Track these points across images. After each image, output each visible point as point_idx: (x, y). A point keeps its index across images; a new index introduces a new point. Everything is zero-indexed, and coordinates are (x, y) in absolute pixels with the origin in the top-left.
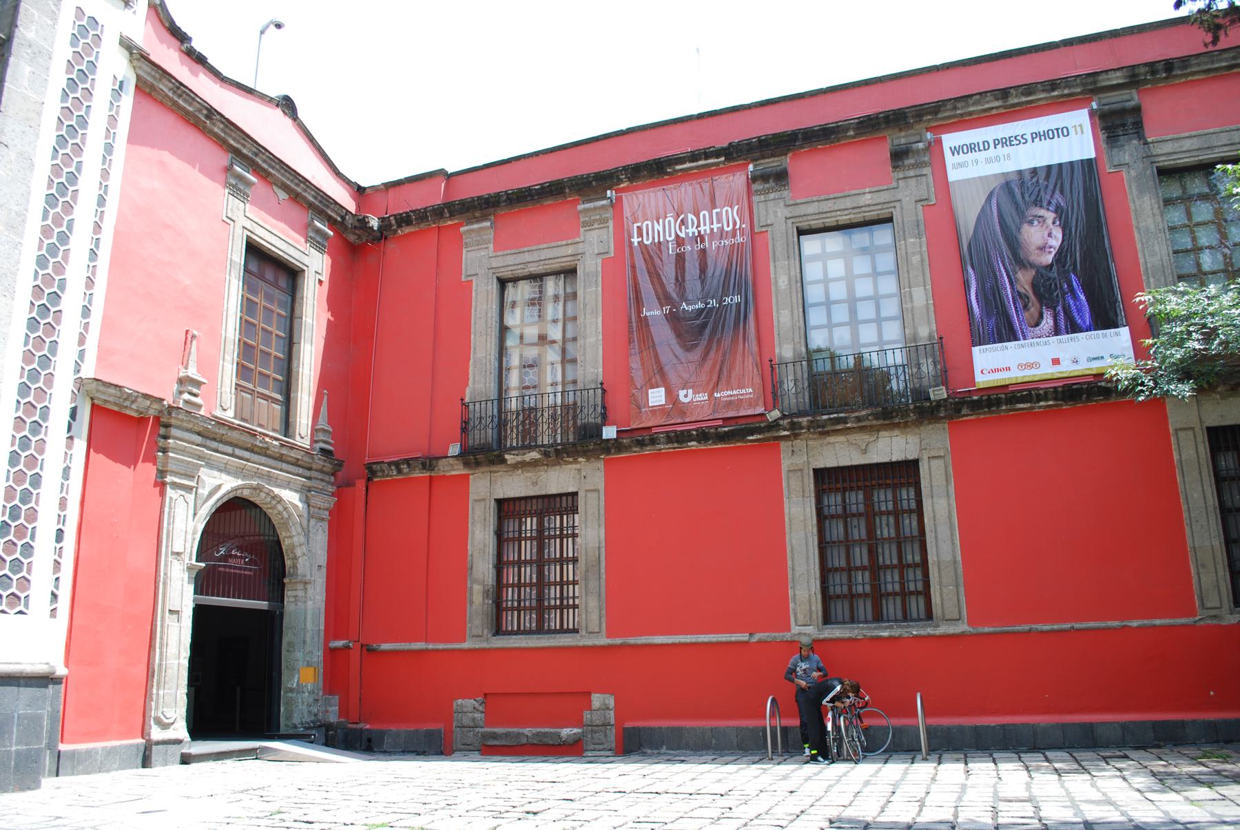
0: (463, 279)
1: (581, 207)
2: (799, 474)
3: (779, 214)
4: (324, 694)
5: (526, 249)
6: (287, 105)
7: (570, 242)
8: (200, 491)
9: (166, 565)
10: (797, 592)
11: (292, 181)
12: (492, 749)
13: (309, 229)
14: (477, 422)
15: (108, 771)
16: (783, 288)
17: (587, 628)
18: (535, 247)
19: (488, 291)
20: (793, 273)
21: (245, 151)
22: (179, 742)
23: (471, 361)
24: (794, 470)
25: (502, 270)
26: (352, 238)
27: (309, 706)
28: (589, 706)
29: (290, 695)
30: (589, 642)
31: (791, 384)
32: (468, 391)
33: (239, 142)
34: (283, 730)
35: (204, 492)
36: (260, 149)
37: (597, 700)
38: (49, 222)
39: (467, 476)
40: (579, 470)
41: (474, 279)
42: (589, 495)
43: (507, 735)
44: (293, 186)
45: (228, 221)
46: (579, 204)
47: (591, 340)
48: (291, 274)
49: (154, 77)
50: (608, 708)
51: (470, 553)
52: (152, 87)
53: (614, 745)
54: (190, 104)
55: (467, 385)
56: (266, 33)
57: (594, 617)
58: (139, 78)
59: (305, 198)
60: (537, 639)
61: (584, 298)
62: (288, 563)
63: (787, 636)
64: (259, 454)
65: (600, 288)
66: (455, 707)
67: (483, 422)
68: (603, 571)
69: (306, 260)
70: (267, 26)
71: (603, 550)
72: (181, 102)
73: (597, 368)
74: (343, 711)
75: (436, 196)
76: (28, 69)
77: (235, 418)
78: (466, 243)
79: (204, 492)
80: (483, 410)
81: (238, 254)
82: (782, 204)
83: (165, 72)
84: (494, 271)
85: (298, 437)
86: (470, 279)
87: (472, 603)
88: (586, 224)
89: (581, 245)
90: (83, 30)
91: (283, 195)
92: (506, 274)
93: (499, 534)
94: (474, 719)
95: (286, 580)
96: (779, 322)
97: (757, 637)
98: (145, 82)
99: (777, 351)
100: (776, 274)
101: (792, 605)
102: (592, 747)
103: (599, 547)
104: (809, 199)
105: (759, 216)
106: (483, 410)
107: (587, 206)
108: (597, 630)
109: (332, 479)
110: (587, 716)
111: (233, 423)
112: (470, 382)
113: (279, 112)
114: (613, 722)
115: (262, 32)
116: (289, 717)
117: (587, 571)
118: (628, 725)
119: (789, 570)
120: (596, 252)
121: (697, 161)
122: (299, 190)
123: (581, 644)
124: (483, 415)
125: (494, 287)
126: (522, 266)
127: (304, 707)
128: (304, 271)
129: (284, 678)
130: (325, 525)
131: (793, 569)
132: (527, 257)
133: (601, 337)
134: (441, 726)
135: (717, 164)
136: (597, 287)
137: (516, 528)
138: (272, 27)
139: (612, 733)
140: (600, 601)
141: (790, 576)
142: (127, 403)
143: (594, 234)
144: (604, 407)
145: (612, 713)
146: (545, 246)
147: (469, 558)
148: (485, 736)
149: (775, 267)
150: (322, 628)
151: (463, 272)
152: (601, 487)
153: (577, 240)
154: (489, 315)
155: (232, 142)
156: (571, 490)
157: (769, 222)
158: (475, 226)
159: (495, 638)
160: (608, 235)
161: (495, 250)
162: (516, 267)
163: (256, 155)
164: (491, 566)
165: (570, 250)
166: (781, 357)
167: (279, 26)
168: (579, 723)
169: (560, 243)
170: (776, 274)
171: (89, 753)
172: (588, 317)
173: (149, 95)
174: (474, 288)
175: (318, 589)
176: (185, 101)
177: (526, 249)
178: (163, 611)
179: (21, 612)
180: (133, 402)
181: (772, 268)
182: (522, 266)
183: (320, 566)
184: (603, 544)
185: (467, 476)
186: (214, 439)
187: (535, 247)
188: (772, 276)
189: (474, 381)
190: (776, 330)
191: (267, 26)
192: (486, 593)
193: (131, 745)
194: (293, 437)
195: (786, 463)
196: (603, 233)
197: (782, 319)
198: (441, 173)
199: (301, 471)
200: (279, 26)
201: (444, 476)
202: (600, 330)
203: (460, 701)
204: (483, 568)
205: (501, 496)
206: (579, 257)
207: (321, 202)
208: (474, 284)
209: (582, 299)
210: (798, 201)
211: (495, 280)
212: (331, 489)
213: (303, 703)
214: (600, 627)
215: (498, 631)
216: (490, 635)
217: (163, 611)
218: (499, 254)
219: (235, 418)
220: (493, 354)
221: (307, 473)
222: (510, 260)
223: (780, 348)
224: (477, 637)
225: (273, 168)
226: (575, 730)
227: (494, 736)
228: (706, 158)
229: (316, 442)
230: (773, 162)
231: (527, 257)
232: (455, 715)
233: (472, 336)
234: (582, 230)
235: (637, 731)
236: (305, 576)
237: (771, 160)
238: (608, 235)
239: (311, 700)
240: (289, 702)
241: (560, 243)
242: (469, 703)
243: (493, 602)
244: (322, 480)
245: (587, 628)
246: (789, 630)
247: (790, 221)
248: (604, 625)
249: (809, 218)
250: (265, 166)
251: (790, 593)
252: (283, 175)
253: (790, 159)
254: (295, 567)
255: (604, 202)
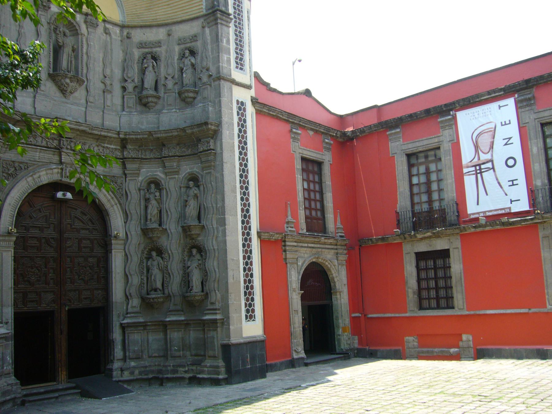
0: (391, 156)
1: (439, 120)
2: (547, 238)
3: (531, 117)
4: (352, 335)
5: (417, 140)
6: (308, 93)
7: (436, 136)
8: (299, 264)
9: (291, 294)
10: (549, 291)
11: (315, 127)
12: (420, 357)
13: (324, 143)
14: (403, 220)
15: (282, 370)
16: (535, 153)
17: (458, 307)
18: (421, 139)
19: (402, 161)
20: (539, 146)
21: (296, 122)
22: (302, 358)
23: (398, 193)
24: (545, 237)
25: (407, 151)
26: (341, 140)
27: (346, 341)
28: (461, 340)
29: (339, 337)
30: (460, 313)
31: (541, 199)
32: (398, 206)
33: (293, 119)
34: (337, 351)
35: (300, 264)
36: (301, 119)
37: (464, 337)
38: (242, 184)
39: (400, 244)
40: (449, 239)
41: (395, 155)
42: (455, 250)
43: (428, 352)
44: (315, 128)
45: (293, 153)
46: (439, 118)
47: (450, 181)
48: (319, 164)
49: (261, 108)
50: (470, 341)
51: (406, 276)
52: (261, 111)
53: (473, 356)
54: (274, 112)
55: (397, 203)
56: (295, 64)
57: (461, 302)
58: (256, 109)
59: (320, 131)
60: (438, 312)
61: (445, 162)
62: (332, 284)
63: (545, 310)
64: (317, 244)
65: (451, 157)
66: (405, 340)
67: (406, 220)
68: (463, 283)
69: (324, 157)
70: (295, 61)
71: (462, 274)
72: (271, 113)
73: (453, 194)
74: (360, 342)
75: (372, 120)
76: (228, 132)
77: (307, 232)
78: (390, 139)
79: (300, 264)
80: (405, 214)
81: (298, 165)
82: (532, 112)
83: (265, 104)
84: (404, 151)
85: (330, 233)
86: (393, 155)
87: (409, 297)
88: (442, 127)
89: (441, 137)
90: (240, 109)
91: (311, 133)
92: (409, 151)
93: (417, 267)
94: (414, 345)
95: (332, 291)
96: (534, 169)
97: (533, 310)
98: (258, 110)
99: (534, 183)
100: (531, 146)
101: (547, 297)
102: (464, 356)
103: (461, 273)
104: (545, 109)
105: (522, 119)
106: (405, 214)
107: (442, 119)
108: (462, 308)
109: (345, 247)
110: (461, 344)
111: (306, 234)
112: (399, 202)
113: (305, 96)
114: (472, 346)
115: (293, 64)
116: (340, 346)
117: (456, 283)
118: (478, 347)
119: (545, 281)
120: (448, 140)
121: (490, 94)
122: (317, 129)
123: (456, 314)
124: (406, 217)
125: (405, 159)
126: (416, 148)
127: (345, 342)
128: (323, 162)
129: (336, 331)
130: (345, 267)
131: (547, 281)
132: (418, 144)
133: (454, 180)
134: (400, 348)
135: (500, 95)
136: (450, 156)
137: (425, 265)
138: (297, 62)
139: (472, 351)
140: (463, 295)
141: (545, 284)
142: (271, 237)
143: (447, 131)
144: (458, 212)
145: (471, 342)
146: (425, 138)
147: (406, 278)
148: (419, 352)
149: (531, 143)
150: (348, 309)
151: (390, 152)
152: (460, 246)
153: (439, 135)
154: (404, 172)
155: (290, 120)
156: (446, 248)
157: (527, 121)
158: (393, 131)
159: (419, 311)
160: (453, 132)
161: (403, 142)
162: (413, 149)
163: (300, 122)
164: (415, 281)
165: (436, 140)
166: (536, 186)
167: (300, 61)
168: (458, 347)
169: (431, 137)
170: (531, 146)
171: (275, 364)
172: (447, 170)
173: (260, 113)
174: (396, 160)
175: (345, 294)
176: (273, 112)
177: (417, 140)
178: (292, 311)
179: (254, 320)
180: (273, 236)
181: (529, 144)
182: (416, 148)
183: (345, 284)
184: (462, 271)
185: (400, 244)
186: (301, 242)
187: (421, 139)
188: (530, 147)
189: (400, 202)
190: (533, 173)
191: (295, 61)
192: (414, 293)
193: (288, 361)
194: (328, 233)
195: (541, 234)
196: (450, 130)
197: (535, 168)
198: (375, 106)
199: (333, 247)
200: (300, 61)
201: (391, 243)
202: (453, 176)
203: (407, 338)
204: (412, 283)
205: (417, 251)
206: (441, 143)
207: (326, 131)
208: (396, 157)
209: (444, 162)
210: (540, 110)
211: (405, 155)
212: (345, 252)
213: (344, 340)
214: (464, 307)
215: (421, 308)
216: (417, 310)
217: (292, 311)
218: (405, 143)
219: (307, 232)
220: (407, 189)
221: (335, 247)
222: (410, 146)
223: (535, 182)
224: (412, 311)
225: (307, 124)
226: (456, 350)
227: (423, 352)
228: (495, 93)
229: (337, 233)
230: (527, 92)
231: (418, 144)
232: (406, 343)
233: (397, 182)
234: (441, 130)
235: (482, 350)
236: (339, 289)
237: (526, 91)
238: (453, 132)
239: (347, 339)
240: (339, 340)
241: (431, 137)
242: (411, 338)
243: (418, 296)
244: (342, 249)
245: (458, 307)
246: (546, 307)
247: (536, 121)
248: (465, 306)
249: (546, 118)
250: (304, 125)
251: (546, 291)
252: (310, 125)
253: (535, 89)
254: (335, 286)
255: (450, 117)
